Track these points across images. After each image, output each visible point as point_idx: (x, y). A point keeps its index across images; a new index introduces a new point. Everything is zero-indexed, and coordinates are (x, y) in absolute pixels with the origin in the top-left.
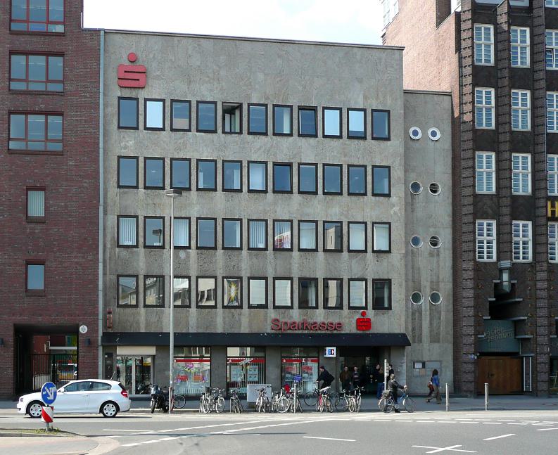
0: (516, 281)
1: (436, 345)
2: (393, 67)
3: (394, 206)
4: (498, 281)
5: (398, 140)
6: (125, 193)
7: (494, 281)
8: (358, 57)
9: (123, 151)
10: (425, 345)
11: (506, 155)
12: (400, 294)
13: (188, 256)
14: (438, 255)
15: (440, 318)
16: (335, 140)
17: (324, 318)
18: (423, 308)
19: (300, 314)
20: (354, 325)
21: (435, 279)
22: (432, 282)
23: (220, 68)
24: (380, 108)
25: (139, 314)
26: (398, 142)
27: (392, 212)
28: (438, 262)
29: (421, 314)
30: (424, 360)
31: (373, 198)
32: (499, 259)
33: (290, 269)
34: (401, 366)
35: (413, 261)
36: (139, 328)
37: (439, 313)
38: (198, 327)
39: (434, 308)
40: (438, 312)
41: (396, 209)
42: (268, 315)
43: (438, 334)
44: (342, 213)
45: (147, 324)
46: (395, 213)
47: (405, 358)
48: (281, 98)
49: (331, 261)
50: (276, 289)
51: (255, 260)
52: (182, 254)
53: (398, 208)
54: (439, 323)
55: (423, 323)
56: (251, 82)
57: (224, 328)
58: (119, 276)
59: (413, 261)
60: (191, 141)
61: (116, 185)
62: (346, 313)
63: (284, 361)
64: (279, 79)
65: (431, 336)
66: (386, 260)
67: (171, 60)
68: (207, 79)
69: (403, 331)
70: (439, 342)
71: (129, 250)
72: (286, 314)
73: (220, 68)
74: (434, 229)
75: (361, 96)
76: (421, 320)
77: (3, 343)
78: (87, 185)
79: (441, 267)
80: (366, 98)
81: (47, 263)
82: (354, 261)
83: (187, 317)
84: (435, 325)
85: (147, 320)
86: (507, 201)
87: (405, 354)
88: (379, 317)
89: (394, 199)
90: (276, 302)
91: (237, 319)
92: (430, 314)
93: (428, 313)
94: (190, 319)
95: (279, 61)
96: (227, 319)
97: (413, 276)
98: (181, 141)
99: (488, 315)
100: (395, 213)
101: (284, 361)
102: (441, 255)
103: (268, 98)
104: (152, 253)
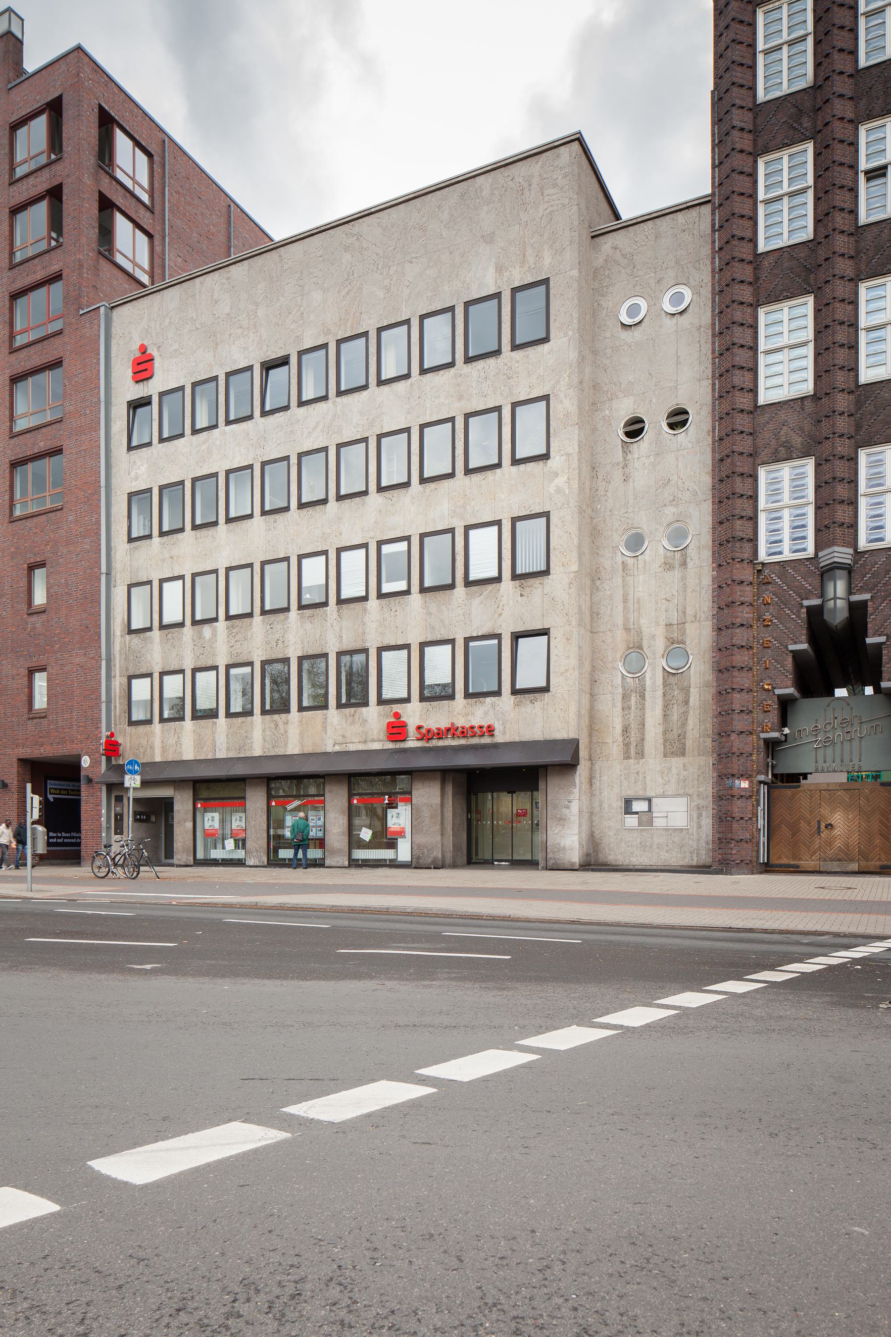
0: (866, 596)
1: (676, 762)
2: (555, 185)
3: (556, 475)
4: (816, 602)
5: (565, 335)
6: (136, 548)
7: (806, 603)
8: (486, 193)
9: (134, 483)
10: (651, 761)
11: (841, 289)
12: (568, 657)
13: (214, 634)
14: (684, 564)
15: (686, 702)
16: (441, 372)
17: (420, 718)
18: (648, 682)
19: (379, 715)
20: (383, 735)
21: (675, 618)
22: (669, 625)
23: (257, 304)
24: (530, 279)
25: (152, 733)
26: (565, 339)
27: (552, 489)
28: (683, 579)
29: (643, 696)
30: (649, 794)
31: (514, 469)
32: (818, 547)
33: (364, 633)
34: (568, 807)
35: (625, 585)
36: (153, 756)
37: (686, 691)
38: (228, 749)
39: (673, 680)
40: (682, 689)
41: (561, 481)
42: (329, 720)
43: (682, 737)
44: (455, 512)
45: (164, 749)
46: (559, 490)
47: (576, 791)
48: (349, 324)
49: (433, 608)
50: (406, 669)
51: (308, 626)
52: (207, 630)
53: (565, 478)
54: (685, 714)
55: (648, 714)
56: (302, 314)
57: (264, 747)
58: (130, 678)
59: (625, 585)
60: (218, 443)
61: (126, 539)
62: (461, 707)
63: (273, 804)
64: (346, 290)
65: (665, 741)
66: (539, 591)
67: (192, 318)
68: (239, 331)
69: (572, 735)
70: (683, 754)
71: (141, 635)
72: (357, 717)
73: (257, 304)
74: (673, 509)
75: (492, 270)
76: (643, 709)
77: (5, 785)
78: (88, 547)
79: (689, 590)
80: (500, 269)
81: (49, 669)
82: (476, 602)
83: (213, 733)
84: (675, 717)
85: (163, 742)
86: (842, 402)
87: (577, 781)
88: (523, 710)
89: (556, 461)
90: (384, 692)
91: (282, 731)
92: (664, 695)
93: (660, 693)
94: (217, 736)
95: (347, 257)
96: (268, 733)
97: (626, 620)
98: (204, 447)
99: (789, 683)
100: (559, 490)
101: (273, 804)
102: (690, 564)
103: (328, 332)
104: (169, 636)
